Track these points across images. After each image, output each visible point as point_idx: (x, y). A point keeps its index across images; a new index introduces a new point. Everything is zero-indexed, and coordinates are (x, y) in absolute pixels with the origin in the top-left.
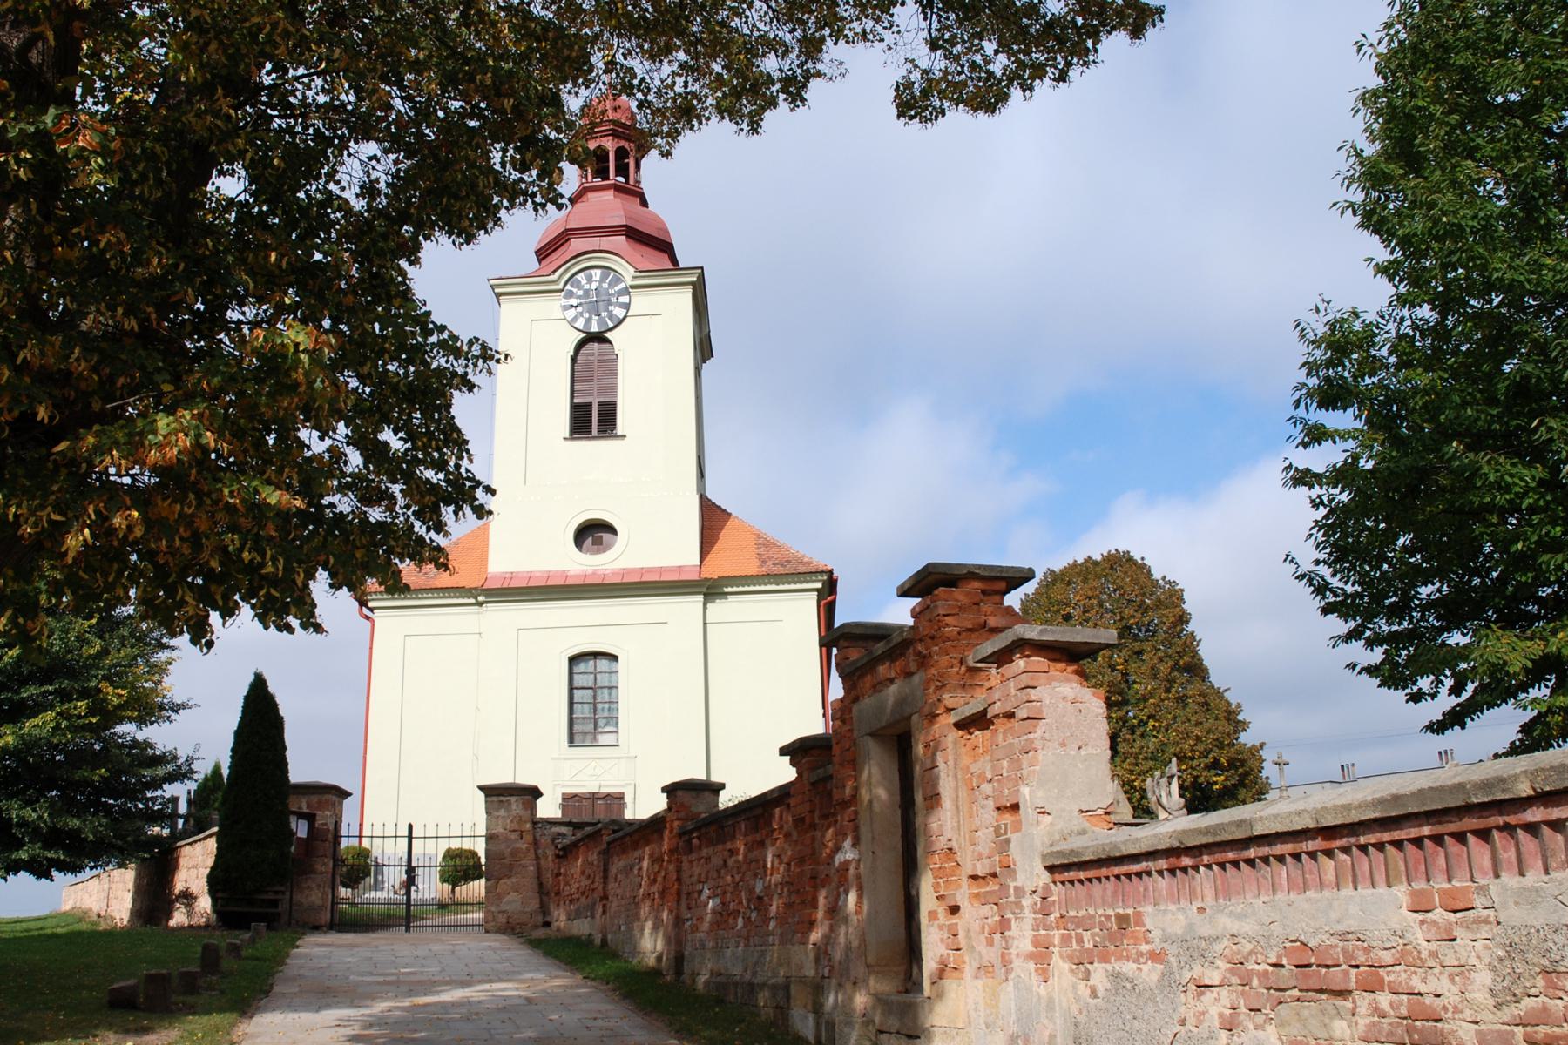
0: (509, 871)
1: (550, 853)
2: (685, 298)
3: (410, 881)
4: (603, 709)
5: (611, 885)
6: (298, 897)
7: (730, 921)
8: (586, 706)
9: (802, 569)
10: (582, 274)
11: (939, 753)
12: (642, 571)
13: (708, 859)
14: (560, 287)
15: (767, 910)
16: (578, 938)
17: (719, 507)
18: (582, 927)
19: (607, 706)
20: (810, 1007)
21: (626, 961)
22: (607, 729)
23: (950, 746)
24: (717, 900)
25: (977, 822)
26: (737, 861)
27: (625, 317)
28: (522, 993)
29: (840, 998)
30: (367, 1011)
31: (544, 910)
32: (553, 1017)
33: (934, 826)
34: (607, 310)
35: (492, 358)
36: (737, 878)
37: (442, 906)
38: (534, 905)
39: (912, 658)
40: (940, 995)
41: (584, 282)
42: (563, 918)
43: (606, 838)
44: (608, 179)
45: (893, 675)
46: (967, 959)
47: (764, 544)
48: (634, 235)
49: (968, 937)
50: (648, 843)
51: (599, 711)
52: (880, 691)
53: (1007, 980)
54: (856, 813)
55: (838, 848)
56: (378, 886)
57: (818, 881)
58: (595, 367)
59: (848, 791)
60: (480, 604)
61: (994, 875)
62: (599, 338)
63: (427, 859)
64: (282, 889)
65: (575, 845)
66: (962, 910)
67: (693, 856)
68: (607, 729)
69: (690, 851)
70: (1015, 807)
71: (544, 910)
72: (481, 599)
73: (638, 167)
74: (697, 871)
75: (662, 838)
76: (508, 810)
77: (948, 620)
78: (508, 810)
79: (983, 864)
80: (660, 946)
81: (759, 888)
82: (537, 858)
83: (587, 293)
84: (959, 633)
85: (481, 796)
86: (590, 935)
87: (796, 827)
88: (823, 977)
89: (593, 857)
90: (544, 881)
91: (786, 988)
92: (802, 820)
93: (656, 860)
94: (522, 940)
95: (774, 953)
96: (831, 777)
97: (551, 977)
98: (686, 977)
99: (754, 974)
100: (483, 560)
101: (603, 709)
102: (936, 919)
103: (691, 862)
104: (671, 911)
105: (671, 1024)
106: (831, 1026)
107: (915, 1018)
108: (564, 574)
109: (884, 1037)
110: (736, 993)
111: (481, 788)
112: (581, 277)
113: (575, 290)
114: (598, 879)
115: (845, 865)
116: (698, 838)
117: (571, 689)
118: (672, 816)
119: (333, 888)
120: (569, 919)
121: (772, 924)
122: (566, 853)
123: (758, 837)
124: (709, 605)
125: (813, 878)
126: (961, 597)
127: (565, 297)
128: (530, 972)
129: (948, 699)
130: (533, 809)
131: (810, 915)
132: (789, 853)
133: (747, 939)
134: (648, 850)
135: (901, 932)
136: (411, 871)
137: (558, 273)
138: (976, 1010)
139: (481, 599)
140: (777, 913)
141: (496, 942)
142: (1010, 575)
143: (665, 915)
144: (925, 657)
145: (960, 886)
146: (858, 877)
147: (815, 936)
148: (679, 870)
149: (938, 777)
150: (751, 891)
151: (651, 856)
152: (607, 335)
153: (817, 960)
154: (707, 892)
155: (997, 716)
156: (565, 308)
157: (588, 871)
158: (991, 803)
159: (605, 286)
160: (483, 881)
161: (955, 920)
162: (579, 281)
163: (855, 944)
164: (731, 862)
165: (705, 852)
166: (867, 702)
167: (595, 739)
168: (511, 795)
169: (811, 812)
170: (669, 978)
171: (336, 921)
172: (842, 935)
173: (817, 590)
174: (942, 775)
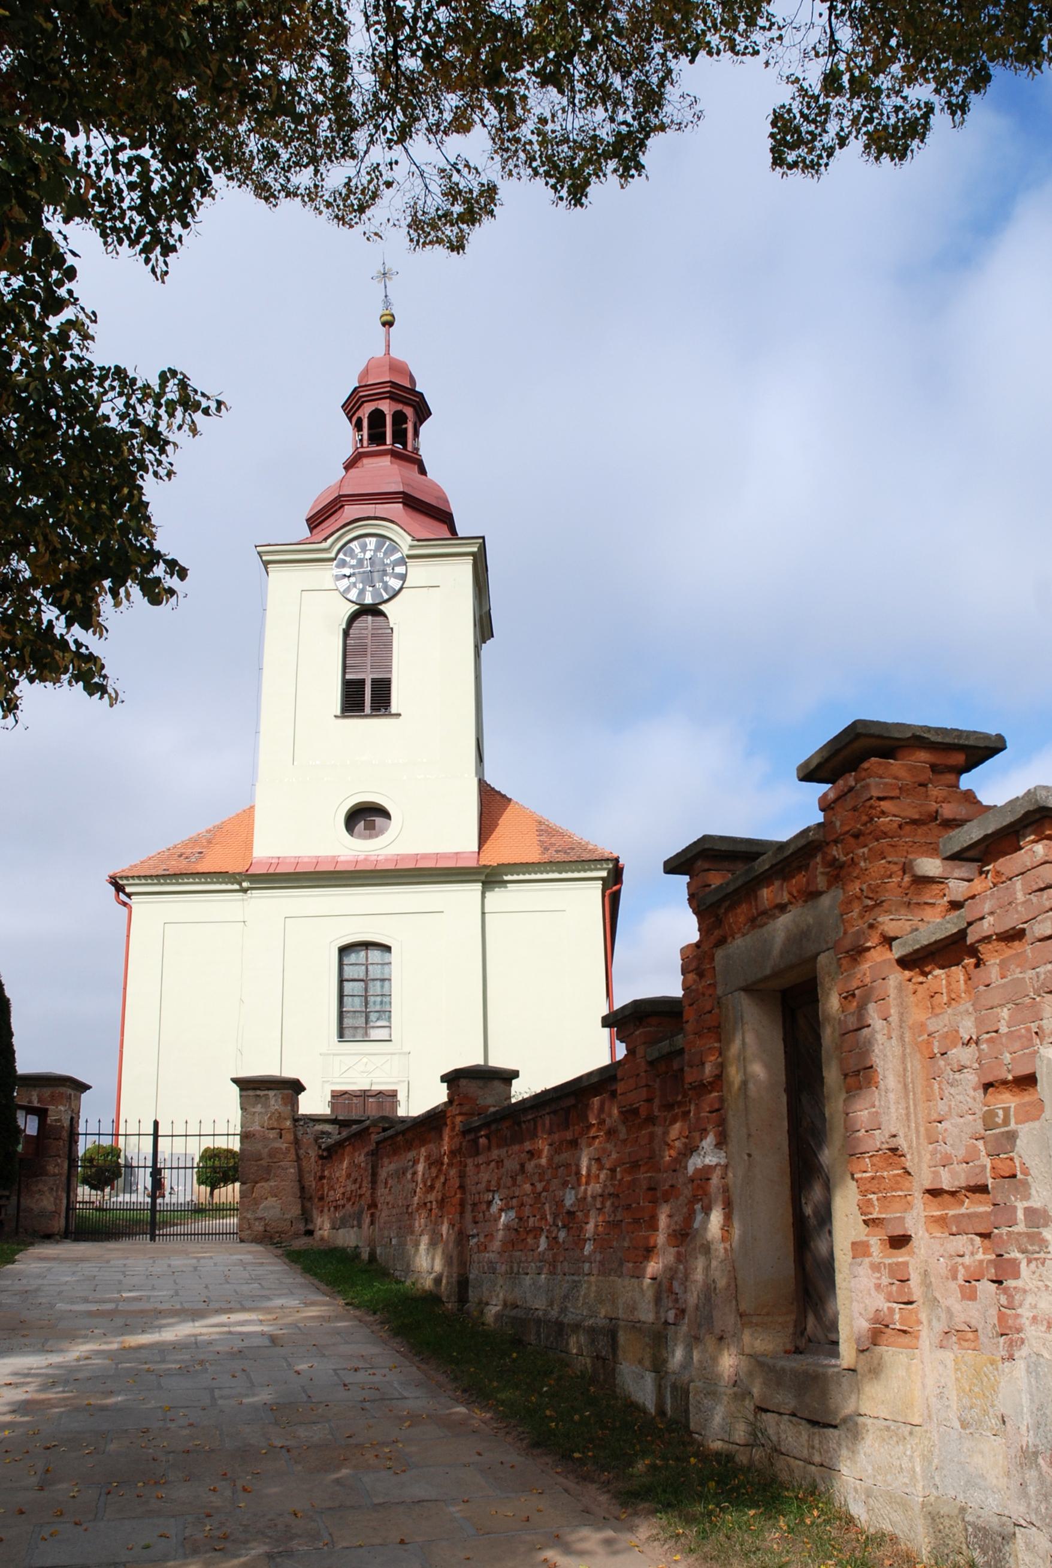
0: (267, 1173)
1: (313, 1153)
2: (464, 569)
3: (157, 1184)
4: (375, 1003)
5: (381, 1191)
6: (26, 1202)
7: (530, 1240)
8: (357, 999)
9: (586, 856)
10: (355, 543)
11: (872, 1007)
12: (416, 857)
13: (500, 1163)
14: (333, 555)
15: (581, 1229)
16: (343, 1250)
17: (499, 793)
18: (347, 1238)
19: (379, 999)
20: (647, 1363)
21: (398, 1282)
22: (379, 1024)
23: (892, 992)
24: (512, 1214)
25: (942, 1107)
26: (538, 1166)
27: (401, 588)
28: (266, 1329)
29: (696, 1356)
30: (55, 1359)
31: (306, 1217)
32: (302, 1367)
33: (862, 1114)
34: (382, 581)
35: (197, 406)
36: (539, 1186)
37: (198, 1211)
38: (295, 1211)
39: (820, 869)
40: (876, 1371)
41: (357, 550)
42: (327, 1225)
43: (374, 1137)
44: (385, 444)
45: (785, 898)
46: (923, 1316)
47: (546, 831)
48: (413, 503)
49: (927, 1284)
50: (424, 1142)
51: (371, 1004)
52: (761, 926)
53: (1011, 1358)
54: (722, 1100)
55: (691, 1149)
56: (130, 1188)
57: (659, 1194)
58: (369, 641)
59: (709, 1070)
60: (245, 891)
61: (983, 1189)
62: (373, 610)
63: (189, 1159)
64: (7, 1193)
65: (340, 1144)
66: (915, 1242)
67: (481, 1159)
68: (379, 1024)
69: (477, 1153)
70: (1028, 1081)
71: (306, 1217)
72: (245, 885)
73: (416, 434)
74: (485, 1176)
75: (441, 1138)
76: (266, 1105)
77: (885, 805)
78: (266, 1105)
79: (954, 1174)
80: (438, 1266)
81: (570, 1199)
82: (298, 1159)
83: (361, 562)
84: (900, 827)
85: (235, 1089)
86: (357, 1247)
87: (625, 1121)
88: (666, 1323)
89: (361, 1158)
90: (307, 1184)
91: (612, 1334)
92: (635, 1112)
93: (434, 1162)
94: (280, 1252)
95: (591, 1285)
96: (681, 1052)
97: (306, 1305)
98: (471, 1306)
99: (563, 1310)
100: (249, 845)
101: (375, 1003)
102: (867, 1254)
103: (478, 1166)
104: (452, 1225)
105: (455, 1379)
106: (682, 1393)
107: (824, 1395)
108: (334, 860)
109: (765, 1416)
110: (538, 1334)
111: (235, 1081)
112: (354, 545)
113: (348, 559)
114: (366, 1184)
115: (705, 1174)
116: (487, 1137)
117: (341, 981)
118: (454, 1110)
119: (70, 1190)
120: (333, 1228)
121: (588, 1248)
122: (330, 1154)
123: (569, 1135)
124: (488, 894)
125: (652, 1189)
126: (902, 773)
127: (338, 566)
128: (280, 1296)
129: (889, 924)
130: (295, 1104)
131: (647, 1238)
132: (614, 1156)
133: (553, 1264)
134: (423, 1151)
135: (789, 1267)
136: (156, 1173)
137: (330, 541)
138: (940, 1396)
139: (245, 885)
140: (596, 1233)
141: (250, 1254)
142: (971, 742)
143: (444, 1229)
144: (842, 866)
145: (909, 1206)
146: (726, 1189)
147: (653, 1267)
148: (462, 1175)
149: (869, 1042)
150: (560, 1203)
151: (427, 1158)
152: (382, 607)
153: (658, 1300)
154: (497, 1203)
155: (987, 939)
156: (339, 578)
157: (354, 1175)
158: (970, 1078)
159: (381, 555)
160: (237, 1185)
161: (900, 1257)
162: (353, 550)
163: (722, 1283)
164: (530, 1166)
165: (495, 1153)
166: (739, 944)
167: (366, 1034)
168: (269, 1089)
169: (649, 1100)
170: (450, 1306)
171: (72, 1228)
172: (700, 1270)
173: (602, 879)
174: (880, 1037)
